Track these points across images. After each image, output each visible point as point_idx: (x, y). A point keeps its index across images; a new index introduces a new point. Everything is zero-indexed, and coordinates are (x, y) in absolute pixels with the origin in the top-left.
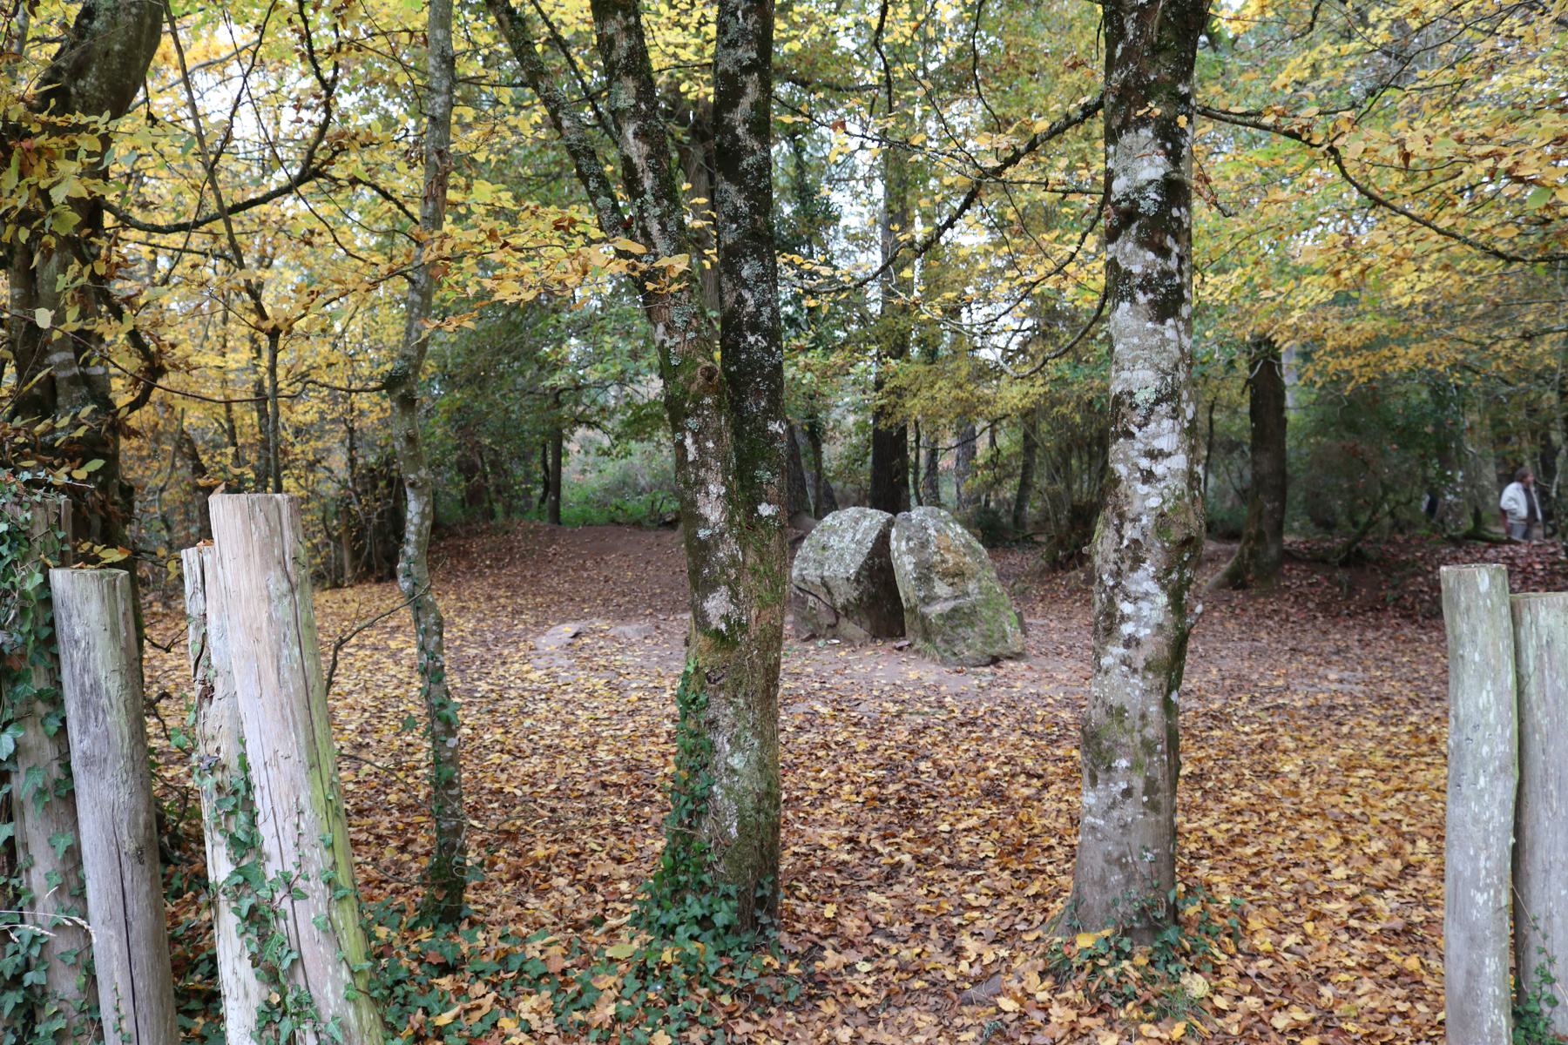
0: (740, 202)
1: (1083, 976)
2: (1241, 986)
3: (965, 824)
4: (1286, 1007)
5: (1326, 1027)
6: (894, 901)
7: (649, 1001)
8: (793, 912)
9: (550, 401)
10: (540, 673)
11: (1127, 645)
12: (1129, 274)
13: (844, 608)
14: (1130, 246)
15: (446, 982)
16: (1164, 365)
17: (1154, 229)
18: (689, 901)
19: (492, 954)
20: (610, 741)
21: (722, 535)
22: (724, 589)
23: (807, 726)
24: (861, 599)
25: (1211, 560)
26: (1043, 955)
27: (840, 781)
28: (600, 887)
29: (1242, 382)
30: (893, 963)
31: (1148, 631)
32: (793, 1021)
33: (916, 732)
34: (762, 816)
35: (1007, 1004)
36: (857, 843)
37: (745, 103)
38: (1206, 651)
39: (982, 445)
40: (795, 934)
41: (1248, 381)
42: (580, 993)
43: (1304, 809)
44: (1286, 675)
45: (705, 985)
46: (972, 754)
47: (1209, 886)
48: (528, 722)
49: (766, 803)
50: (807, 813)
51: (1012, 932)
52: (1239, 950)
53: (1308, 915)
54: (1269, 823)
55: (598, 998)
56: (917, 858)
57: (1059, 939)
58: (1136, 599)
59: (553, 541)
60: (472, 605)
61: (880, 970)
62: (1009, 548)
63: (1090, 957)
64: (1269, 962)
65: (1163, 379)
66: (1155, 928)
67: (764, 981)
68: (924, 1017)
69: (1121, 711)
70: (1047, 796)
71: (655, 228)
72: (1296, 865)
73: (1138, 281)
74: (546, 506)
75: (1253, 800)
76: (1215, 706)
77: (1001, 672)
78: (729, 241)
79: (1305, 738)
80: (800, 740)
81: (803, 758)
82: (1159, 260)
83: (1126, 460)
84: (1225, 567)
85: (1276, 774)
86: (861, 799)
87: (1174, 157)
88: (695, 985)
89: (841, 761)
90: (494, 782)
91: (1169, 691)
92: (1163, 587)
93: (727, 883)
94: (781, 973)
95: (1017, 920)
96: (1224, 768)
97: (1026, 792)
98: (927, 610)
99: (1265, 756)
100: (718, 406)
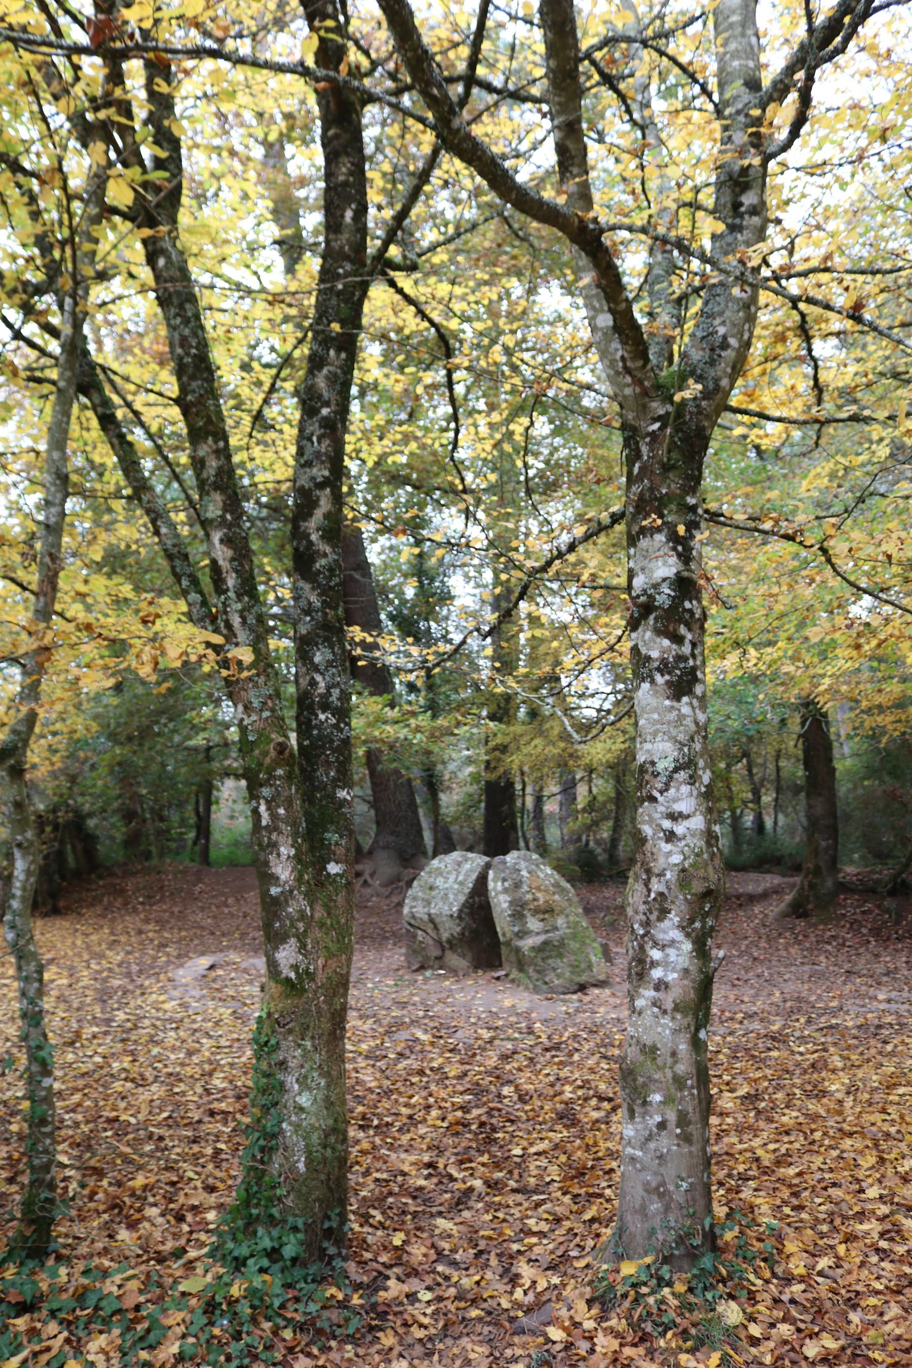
0: (313, 598)
1: (627, 1304)
2: (775, 1312)
3: (537, 1149)
4: (817, 1334)
5: (855, 1355)
6: (461, 1227)
7: (213, 1337)
8: (364, 1241)
9: (201, 757)
10: (174, 1003)
11: (657, 988)
12: (648, 658)
13: (449, 941)
14: (648, 634)
15: (21, 1323)
16: (681, 737)
17: (668, 619)
18: (260, 1234)
19: (71, 1290)
20: (227, 1069)
21: (291, 891)
22: (293, 941)
23: (407, 1052)
24: (463, 934)
25: (776, 892)
26: (590, 1283)
27: (428, 1107)
28: (189, 1218)
29: (795, 736)
30: (452, 1291)
31: (675, 975)
32: (350, 1355)
33: (505, 1057)
34: (329, 1151)
35: (556, 1334)
36: (435, 1168)
37: (319, 514)
38: (771, 975)
39: (582, 791)
40: (362, 1263)
41: (800, 736)
42: (148, 1331)
43: (846, 1127)
44: (840, 996)
45: (269, 1319)
46: (552, 1078)
47: (752, 1208)
48: (155, 1051)
49: (332, 1139)
50: (394, 1139)
51: (565, 1258)
52: (774, 1275)
53: (840, 1237)
54: (813, 1142)
55: (165, 1336)
56: (488, 1184)
57: (605, 1267)
58: (664, 946)
59: (199, 880)
60: (123, 939)
61: (440, 1299)
62: (604, 883)
63: (634, 1286)
64: (802, 1287)
65: (681, 749)
66: (693, 1256)
67: (325, 1314)
68: (477, 1348)
69: (654, 1049)
70: (615, 1118)
71: (236, 621)
72: (834, 1185)
73: (656, 664)
74: (197, 848)
75: (801, 1120)
76: (775, 1028)
77: (587, 999)
78: (304, 632)
79: (853, 1057)
80: (400, 1066)
81: (399, 1084)
82: (674, 646)
83: (651, 821)
84: (788, 898)
85: (824, 1093)
86: (445, 1125)
87: (686, 557)
88: (261, 1319)
89: (433, 1087)
90: (113, 1110)
91: (697, 1030)
92: (688, 935)
93: (295, 1216)
94: (343, 1305)
95: (572, 1245)
96: (778, 1088)
97: (595, 1115)
98: (520, 943)
99: (815, 1076)
100: (289, 777)
